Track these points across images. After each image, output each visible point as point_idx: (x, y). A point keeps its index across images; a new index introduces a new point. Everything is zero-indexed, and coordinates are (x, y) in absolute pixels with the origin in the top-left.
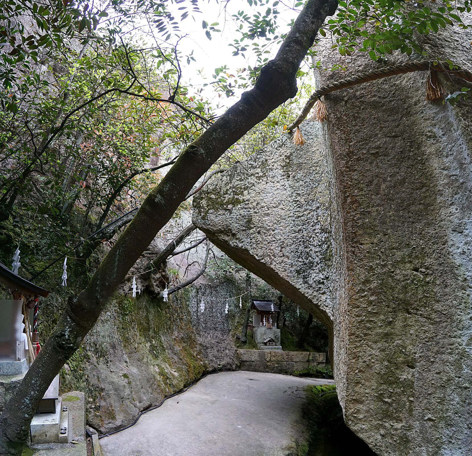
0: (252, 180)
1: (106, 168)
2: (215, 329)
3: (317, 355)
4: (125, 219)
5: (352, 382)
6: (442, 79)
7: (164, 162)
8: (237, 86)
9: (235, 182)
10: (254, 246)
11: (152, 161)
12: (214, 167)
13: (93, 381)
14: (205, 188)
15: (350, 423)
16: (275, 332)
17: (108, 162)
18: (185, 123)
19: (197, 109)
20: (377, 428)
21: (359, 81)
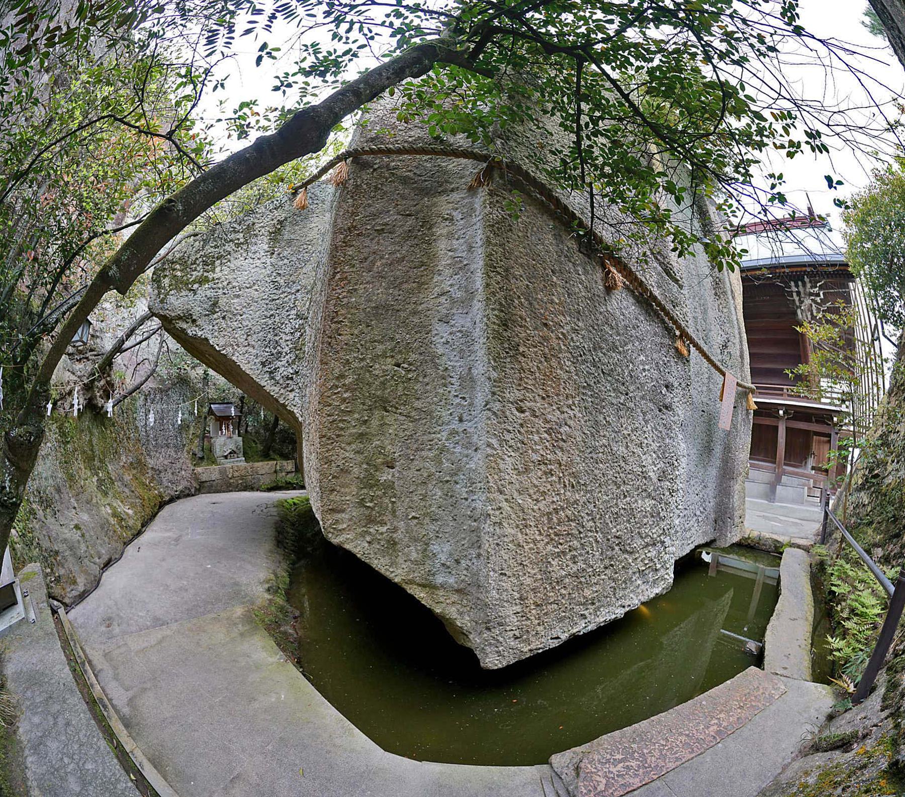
0: (229, 247)
1: (61, 229)
2: (167, 446)
3: (285, 463)
4: (71, 301)
5: (327, 490)
6: (496, 175)
7: (130, 220)
8: (256, 127)
9: (209, 249)
10: (216, 334)
11: (118, 218)
12: (189, 229)
13: (45, 544)
14: (170, 257)
15: (330, 535)
16: (236, 442)
17: (65, 221)
18: (172, 168)
19: (193, 151)
20: (363, 535)
21: (400, 152)
